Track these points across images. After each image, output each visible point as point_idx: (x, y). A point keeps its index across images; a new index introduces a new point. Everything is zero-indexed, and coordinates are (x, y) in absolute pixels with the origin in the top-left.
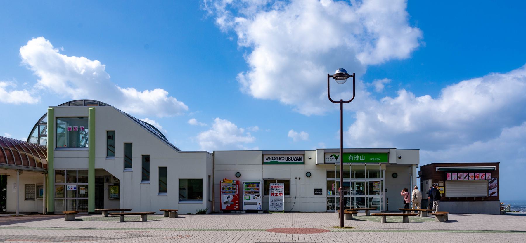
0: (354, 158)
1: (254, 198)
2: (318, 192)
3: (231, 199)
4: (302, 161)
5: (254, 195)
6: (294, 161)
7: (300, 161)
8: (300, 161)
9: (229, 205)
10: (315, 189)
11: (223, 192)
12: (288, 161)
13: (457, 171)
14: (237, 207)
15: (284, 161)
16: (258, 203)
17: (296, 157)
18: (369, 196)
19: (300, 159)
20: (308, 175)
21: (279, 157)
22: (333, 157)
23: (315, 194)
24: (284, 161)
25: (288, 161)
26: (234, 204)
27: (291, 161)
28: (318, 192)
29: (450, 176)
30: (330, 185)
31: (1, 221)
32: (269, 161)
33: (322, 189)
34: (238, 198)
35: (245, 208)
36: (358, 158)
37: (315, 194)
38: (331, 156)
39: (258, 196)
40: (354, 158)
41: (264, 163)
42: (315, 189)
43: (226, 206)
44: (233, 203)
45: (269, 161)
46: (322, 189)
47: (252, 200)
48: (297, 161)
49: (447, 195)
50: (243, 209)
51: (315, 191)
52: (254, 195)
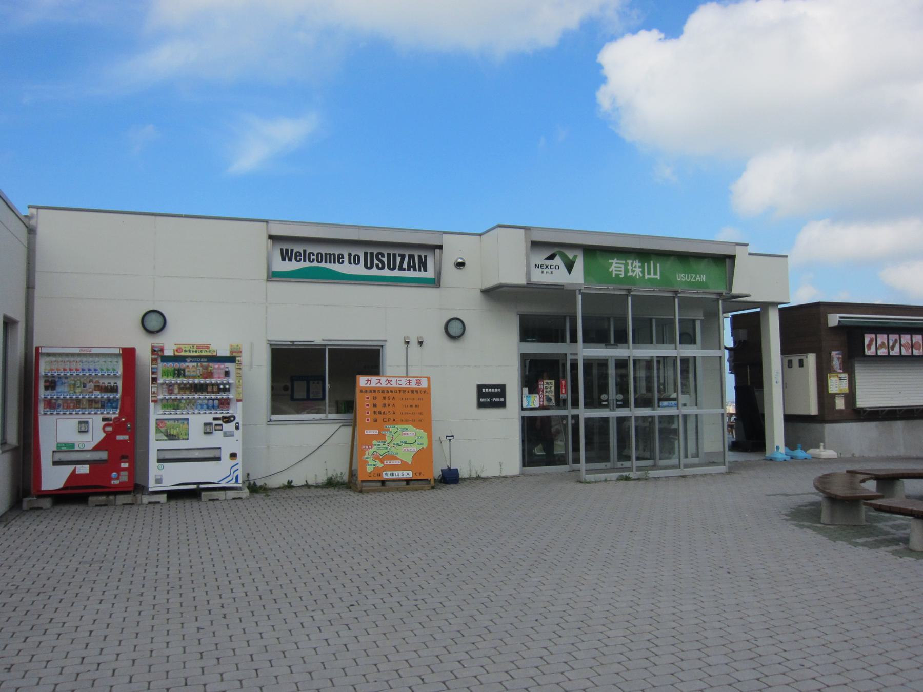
0: (626, 271)
1: (208, 429)
2: (490, 397)
3: (97, 434)
4: (430, 274)
5: (208, 418)
6: (397, 273)
7: (421, 274)
8: (421, 274)
9: (84, 469)
10: (480, 387)
11: (51, 405)
12: (374, 272)
13: (888, 329)
14: (124, 476)
15: (359, 270)
16: (225, 456)
17: (405, 258)
18: (612, 414)
19: (423, 265)
20: (454, 330)
21: (336, 251)
22: (558, 261)
23: (481, 405)
24: (359, 270)
25: (374, 272)
26: (112, 465)
27: (386, 272)
28: (490, 397)
29: (874, 344)
30: (534, 372)
31: (917, 338)
32: (293, 266)
33: (503, 387)
34: (124, 444)
35: (165, 476)
36: (638, 271)
37: (481, 405)
38: (552, 257)
39: (228, 420)
40: (626, 271)
41: (274, 276)
42: (480, 387)
43: (67, 470)
44: (103, 455)
45: (293, 266)
46: (503, 387)
47: (197, 439)
48: (412, 274)
49: (863, 402)
50: (152, 486)
51: (481, 394)
52: (208, 418)
